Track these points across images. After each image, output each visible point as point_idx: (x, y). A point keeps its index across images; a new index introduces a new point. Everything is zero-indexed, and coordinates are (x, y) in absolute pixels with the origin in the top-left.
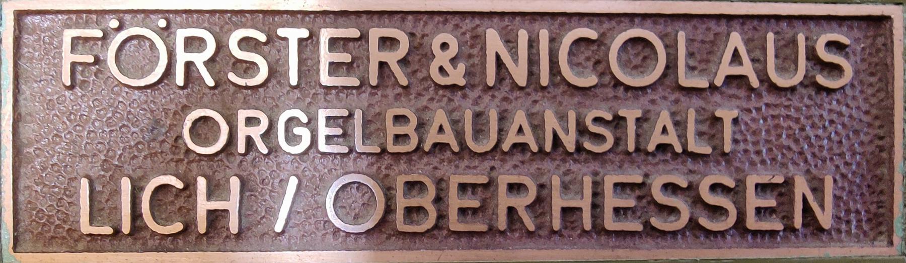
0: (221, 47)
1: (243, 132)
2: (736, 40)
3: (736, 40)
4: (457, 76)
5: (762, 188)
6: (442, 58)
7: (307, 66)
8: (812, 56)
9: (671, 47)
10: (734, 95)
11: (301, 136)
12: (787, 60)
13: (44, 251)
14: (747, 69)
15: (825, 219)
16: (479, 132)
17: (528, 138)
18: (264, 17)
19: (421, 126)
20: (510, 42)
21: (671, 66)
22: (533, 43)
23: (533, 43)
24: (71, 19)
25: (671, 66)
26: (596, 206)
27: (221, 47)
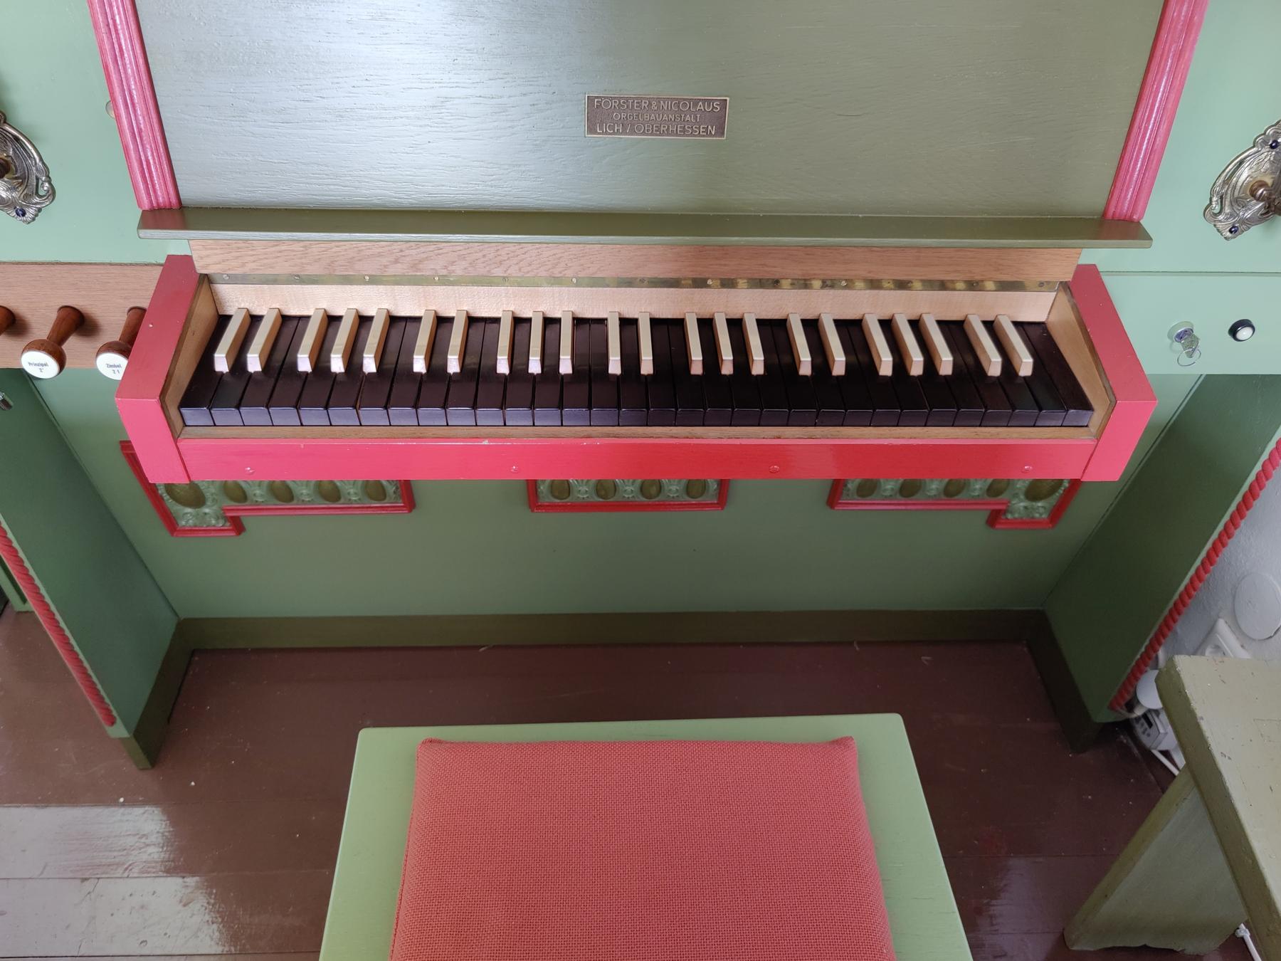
0: (620, 103)
1: (622, 116)
2: (700, 103)
3: (700, 103)
4: (656, 108)
5: (703, 128)
6: (653, 105)
7: (633, 106)
8: (713, 106)
9: (690, 104)
10: (112, 19)
11: (606, 319)
12: (709, 106)
13: (427, 269)
14: (702, 108)
15: (713, 133)
16: (659, 117)
17: (667, 119)
18: (1133, 213)
19: (650, 116)
20: (665, 103)
21: (690, 107)
22: (668, 103)
23: (668, 103)
24: (234, 90)
25: (690, 107)
26: (677, 130)
27: (620, 103)
